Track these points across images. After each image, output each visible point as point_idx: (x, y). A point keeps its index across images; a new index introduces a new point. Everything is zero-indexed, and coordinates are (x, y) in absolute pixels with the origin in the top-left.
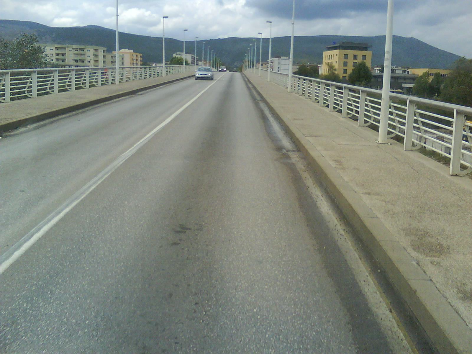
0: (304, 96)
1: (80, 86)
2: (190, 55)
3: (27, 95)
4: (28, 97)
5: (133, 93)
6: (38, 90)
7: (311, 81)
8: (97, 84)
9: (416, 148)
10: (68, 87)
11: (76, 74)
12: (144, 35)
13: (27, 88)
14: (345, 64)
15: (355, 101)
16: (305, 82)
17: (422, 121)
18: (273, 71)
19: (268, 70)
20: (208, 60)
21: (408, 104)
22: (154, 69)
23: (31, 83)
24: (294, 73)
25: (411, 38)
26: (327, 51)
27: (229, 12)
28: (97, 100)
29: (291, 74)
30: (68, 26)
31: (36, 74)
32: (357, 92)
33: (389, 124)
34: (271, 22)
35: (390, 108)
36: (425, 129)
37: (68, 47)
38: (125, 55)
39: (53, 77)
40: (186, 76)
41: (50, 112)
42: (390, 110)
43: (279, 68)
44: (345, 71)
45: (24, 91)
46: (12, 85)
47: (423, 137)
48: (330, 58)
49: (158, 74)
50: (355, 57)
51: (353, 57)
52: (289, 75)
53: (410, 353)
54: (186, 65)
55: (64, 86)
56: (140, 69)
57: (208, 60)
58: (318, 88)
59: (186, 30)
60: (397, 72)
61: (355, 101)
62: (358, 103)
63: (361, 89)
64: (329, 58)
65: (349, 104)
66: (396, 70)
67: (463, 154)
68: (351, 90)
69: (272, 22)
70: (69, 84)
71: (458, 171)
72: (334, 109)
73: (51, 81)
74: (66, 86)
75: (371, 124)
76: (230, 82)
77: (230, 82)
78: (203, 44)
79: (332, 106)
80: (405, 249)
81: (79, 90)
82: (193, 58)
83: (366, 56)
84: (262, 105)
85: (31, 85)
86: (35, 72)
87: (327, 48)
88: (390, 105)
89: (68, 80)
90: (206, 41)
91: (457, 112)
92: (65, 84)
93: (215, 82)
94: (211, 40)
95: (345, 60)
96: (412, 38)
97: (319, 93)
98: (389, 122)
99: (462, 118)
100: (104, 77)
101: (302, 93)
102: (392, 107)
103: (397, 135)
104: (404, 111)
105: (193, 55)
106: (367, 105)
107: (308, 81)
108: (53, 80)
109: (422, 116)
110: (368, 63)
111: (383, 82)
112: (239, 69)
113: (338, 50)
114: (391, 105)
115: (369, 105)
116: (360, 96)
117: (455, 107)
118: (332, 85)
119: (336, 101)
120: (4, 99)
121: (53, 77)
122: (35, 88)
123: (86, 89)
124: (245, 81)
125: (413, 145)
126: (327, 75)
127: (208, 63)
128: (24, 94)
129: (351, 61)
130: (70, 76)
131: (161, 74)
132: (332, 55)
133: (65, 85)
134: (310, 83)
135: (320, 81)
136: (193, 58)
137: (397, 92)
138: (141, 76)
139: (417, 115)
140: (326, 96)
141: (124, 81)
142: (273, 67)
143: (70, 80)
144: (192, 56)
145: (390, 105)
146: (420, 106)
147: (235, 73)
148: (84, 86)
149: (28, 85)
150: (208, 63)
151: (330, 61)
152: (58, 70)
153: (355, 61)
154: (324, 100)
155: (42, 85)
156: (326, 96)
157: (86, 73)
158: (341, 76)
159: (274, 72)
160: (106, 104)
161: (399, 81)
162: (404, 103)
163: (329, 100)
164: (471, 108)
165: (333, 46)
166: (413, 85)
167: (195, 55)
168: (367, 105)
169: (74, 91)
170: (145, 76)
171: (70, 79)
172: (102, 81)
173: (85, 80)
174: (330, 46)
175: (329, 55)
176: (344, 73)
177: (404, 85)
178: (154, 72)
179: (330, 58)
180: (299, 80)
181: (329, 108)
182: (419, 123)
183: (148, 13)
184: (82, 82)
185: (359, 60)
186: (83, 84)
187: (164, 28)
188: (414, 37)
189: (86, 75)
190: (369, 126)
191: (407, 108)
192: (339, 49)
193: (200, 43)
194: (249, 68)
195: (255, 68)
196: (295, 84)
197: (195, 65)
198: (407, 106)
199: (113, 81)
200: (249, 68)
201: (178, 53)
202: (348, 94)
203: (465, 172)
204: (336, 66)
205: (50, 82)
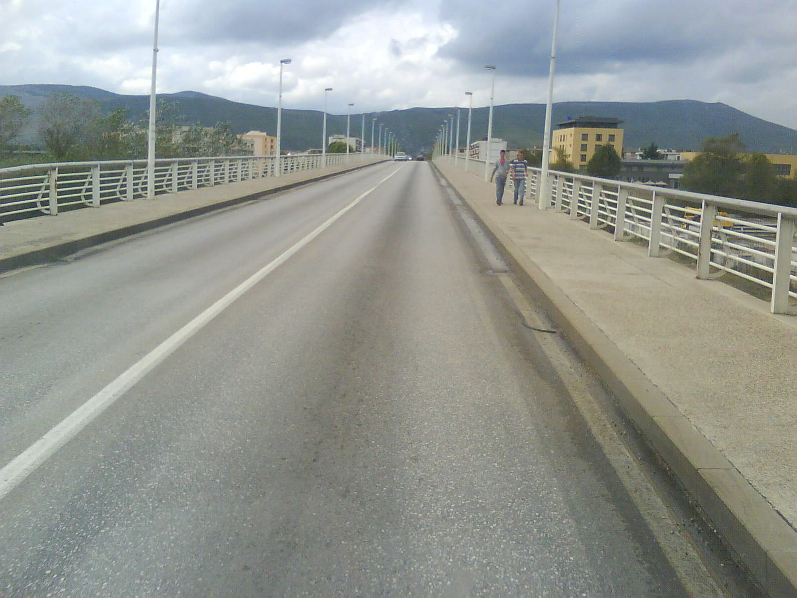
0: (534, 199)
1: (116, 197)
2: (355, 138)
3: (83, 203)
4: (43, 213)
5: (255, 197)
6: (102, 195)
7: (570, 180)
9: (628, 238)
10: (167, 187)
12: (273, 107)
13: (140, 184)
14: (584, 148)
15: (610, 204)
16: (535, 177)
20: (380, 145)
21: (619, 191)
22: (291, 161)
23: (90, 183)
25: (717, 103)
26: (558, 129)
27: (408, 66)
28: (226, 202)
32: (648, 195)
33: (579, 207)
34: (471, 94)
38: (255, 139)
39: (91, 178)
41: (20, 256)
42: (663, 215)
44: (583, 158)
45: (36, 202)
49: (297, 168)
50: (599, 137)
51: (595, 137)
52: (542, 173)
56: (264, 161)
57: (380, 145)
58: (567, 189)
59: (331, 89)
60: (669, 157)
61: (610, 204)
62: (615, 205)
64: (561, 139)
66: (667, 155)
67: (663, 236)
68: (605, 187)
69: (473, 94)
72: (562, 209)
73: (168, 176)
76: (408, 188)
78: (373, 122)
79: (595, 220)
80: (640, 370)
81: (202, 188)
84: (449, 191)
85: (48, 191)
86: (55, 169)
87: (557, 125)
88: (627, 199)
89: (86, 186)
91: (595, 183)
92: (115, 190)
95: (584, 143)
96: (719, 104)
99: (712, 211)
100: (138, 181)
102: (629, 201)
103: (609, 225)
104: (649, 206)
106: (602, 202)
108: (223, 170)
109: (636, 203)
110: (618, 147)
111: (543, 160)
112: (428, 157)
113: (574, 128)
114: (629, 199)
115: (671, 219)
116: (617, 194)
117: (705, 197)
118: (596, 183)
120: (91, 203)
121: (91, 178)
122: (96, 193)
124: (482, 267)
125: (626, 234)
126: (554, 164)
127: (380, 150)
128: (36, 207)
129: (592, 144)
130: (170, 171)
131: (272, 168)
132: (564, 136)
133: (115, 192)
134: (630, 197)
135: (536, 170)
136: (358, 142)
137: (657, 186)
138: (287, 169)
139: (667, 211)
141: (173, 191)
142: (478, 154)
143: (170, 178)
144: (357, 141)
145: (663, 208)
147: (421, 162)
149: (86, 186)
150: (380, 150)
151: (562, 143)
153: (598, 143)
154: (562, 203)
157: (92, 175)
158: (577, 166)
161: (665, 170)
162: (590, 184)
164: (795, 209)
166: (681, 175)
167: (361, 138)
169: (99, 207)
170: (285, 170)
171: (191, 173)
172: (230, 177)
173: (170, 180)
174: (562, 123)
175: (561, 136)
177: (671, 176)
178: (292, 165)
180: (556, 180)
182: (722, 236)
184: (83, 193)
185: (604, 142)
186: (188, 183)
187: (156, 51)
188: (723, 102)
189: (209, 167)
191: (777, 230)
192: (575, 127)
193: (369, 116)
194: (446, 154)
200: (446, 154)
201: (336, 136)
203: (664, 253)
204: (569, 151)
205: (167, 177)
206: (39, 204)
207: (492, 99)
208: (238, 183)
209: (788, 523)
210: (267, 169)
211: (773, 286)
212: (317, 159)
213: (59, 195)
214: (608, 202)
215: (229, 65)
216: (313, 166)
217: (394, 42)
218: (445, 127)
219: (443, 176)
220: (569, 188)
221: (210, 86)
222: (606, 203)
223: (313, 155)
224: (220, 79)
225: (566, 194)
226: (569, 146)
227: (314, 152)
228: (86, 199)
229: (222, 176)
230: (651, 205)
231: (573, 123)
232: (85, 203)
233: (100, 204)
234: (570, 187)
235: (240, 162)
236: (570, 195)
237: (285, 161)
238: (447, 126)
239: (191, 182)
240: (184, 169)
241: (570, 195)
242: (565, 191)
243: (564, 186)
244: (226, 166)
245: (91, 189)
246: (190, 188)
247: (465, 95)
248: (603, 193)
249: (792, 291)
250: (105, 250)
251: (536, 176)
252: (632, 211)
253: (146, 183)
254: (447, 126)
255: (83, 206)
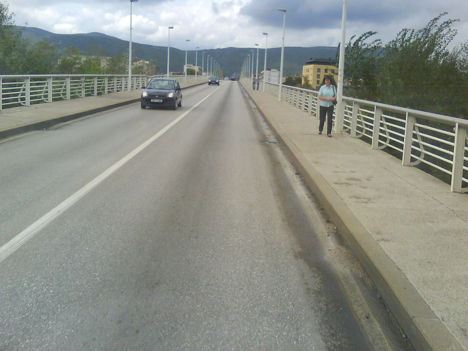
3: (19, 103)
4: (44, 101)
7: (308, 93)
8: (47, 100)
10: (44, 98)
11: (53, 83)
12: (146, 44)
14: (318, 76)
16: (302, 95)
17: (363, 117)
18: (269, 83)
19: (263, 81)
20: (211, 71)
21: (375, 110)
22: (125, 80)
24: (283, 84)
26: (305, 65)
29: (281, 85)
30: (68, 32)
31: (30, 81)
32: (371, 108)
34: (267, 34)
35: (414, 130)
36: (424, 144)
37: (102, 58)
39: (47, 85)
40: (192, 85)
42: (346, 110)
43: (269, 79)
45: (41, 96)
46: (31, 89)
47: (422, 152)
48: (308, 69)
50: (326, 71)
53: (396, 350)
54: (187, 75)
55: (59, 95)
57: (211, 71)
59: (189, 41)
63: (355, 100)
65: (381, 131)
70: (64, 92)
71: (459, 188)
72: (379, 145)
73: (22, 90)
74: (43, 97)
75: (362, 136)
77: (229, 91)
78: (203, 54)
82: (200, 70)
83: (320, 69)
89: (21, 92)
90: (206, 50)
91: (376, 108)
92: (60, 93)
93: (187, 113)
94: (210, 49)
97: (316, 106)
98: (413, 147)
101: (298, 106)
103: (364, 136)
104: (372, 116)
105: (200, 67)
106: (382, 125)
107: (313, 95)
112: (237, 79)
113: (313, 65)
114: (382, 117)
117: (408, 110)
119: (306, 104)
120: (24, 103)
123: (48, 102)
132: (308, 69)
136: (200, 69)
139: (383, 119)
140: (348, 119)
144: (199, 68)
145: (414, 126)
146: (386, 112)
148: (64, 97)
149: (44, 90)
151: (307, 73)
152: (71, 77)
155: (36, 93)
156: (348, 119)
159: (272, 84)
160: (4, 143)
162: (371, 108)
163: (351, 123)
165: (310, 61)
168: (415, 136)
172: (117, 88)
175: (307, 69)
176: (317, 84)
178: (125, 84)
179: (308, 69)
180: (296, 92)
181: (350, 134)
183: (146, 20)
190: (361, 138)
191: (455, 135)
193: (200, 52)
194: (247, 78)
195: (249, 78)
196: (287, 93)
197: (196, 75)
198: (406, 120)
199: (79, 94)
202: (306, 96)
204: (310, 78)
206: (19, 100)
207: (283, 39)
208: (115, 94)
209: (300, 151)
210: (127, 85)
211: (452, 174)
212: (177, 78)
213: (3, 98)
214: (388, 126)
215: (117, 16)
216: (125, 87)
217: (214, 4)
218: (251, 56)
219: (242, 86)
220: (349, 110)
221: (107, 30)
222: (362, 118)
223: (177, 75)
224: (112, 24)
225: (360, 120)
226: (311, 75)
227: (174, 74)
228: (21, 101)
229: (138, 85)
230: (352, 109)
231: (313, 62)
232: (77, 95)
233: (108, 93)
234: (351, 109)
235: (141, 78)
236: (350, 117)
237: (142, 79)
238: (250, 57)
239: (113, 88)
240: (100, 81)
241: (350, 117)
242: (313, 102)
243: (358, 113)
244: (123, 80)
245: (25, 93)
246: (80, 96)
247: (278, 11)
248: (383, 117)
249: (464, 178)
250: (88, 118)
251: (308, 95)
252: (362, 119)
253: (47, 92)
254: (250, 57)
255: (42, 102)
